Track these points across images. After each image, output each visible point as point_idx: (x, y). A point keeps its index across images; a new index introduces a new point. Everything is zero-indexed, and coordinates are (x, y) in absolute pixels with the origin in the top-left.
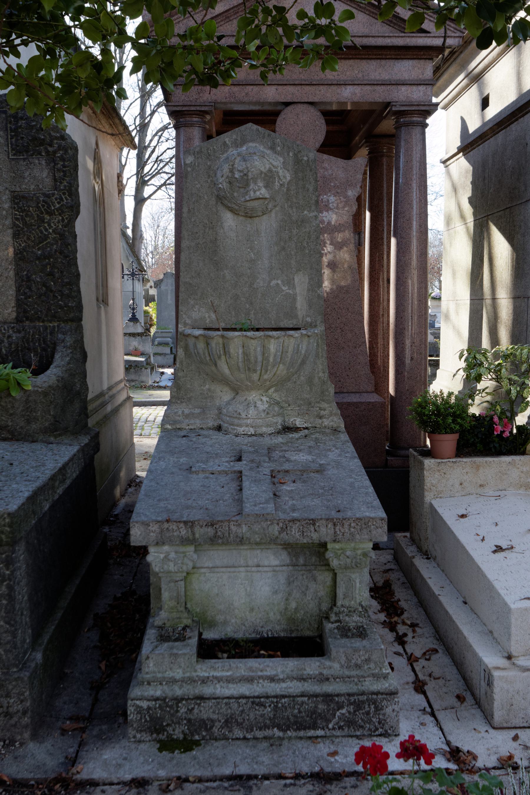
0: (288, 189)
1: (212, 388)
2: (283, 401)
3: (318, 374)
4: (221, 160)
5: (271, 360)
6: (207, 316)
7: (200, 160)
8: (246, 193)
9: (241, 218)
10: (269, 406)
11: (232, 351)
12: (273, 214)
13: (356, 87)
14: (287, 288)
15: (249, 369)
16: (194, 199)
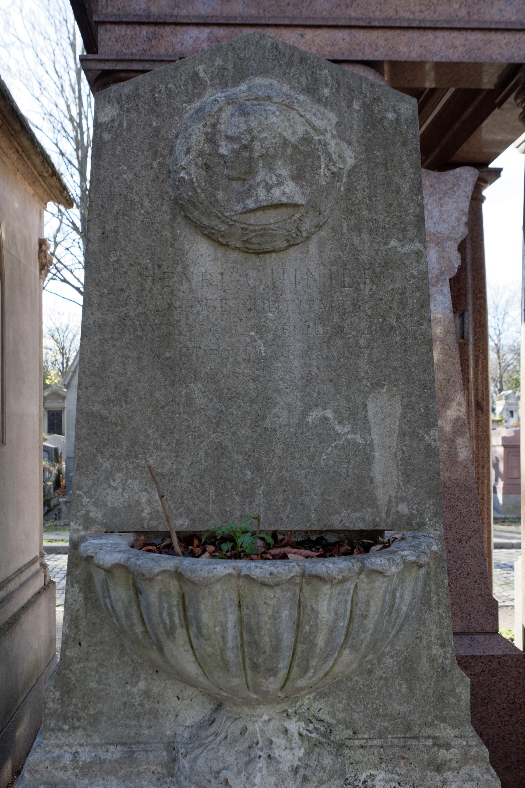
0: (350, 188)
1: (155, 690)
2: (339, 722)
3: (429, 648)
4: (187, 116)
5: (320, 642)
6: (144, 500)
7: (134, 114)
8: (248, 192)
9: (234, 255)
10: (308, 754)
11: (205, 617)
12: (313, 246)
13: (455, 34)
14: (348, 428)
15: (255, 667)
16: (116, 208)
